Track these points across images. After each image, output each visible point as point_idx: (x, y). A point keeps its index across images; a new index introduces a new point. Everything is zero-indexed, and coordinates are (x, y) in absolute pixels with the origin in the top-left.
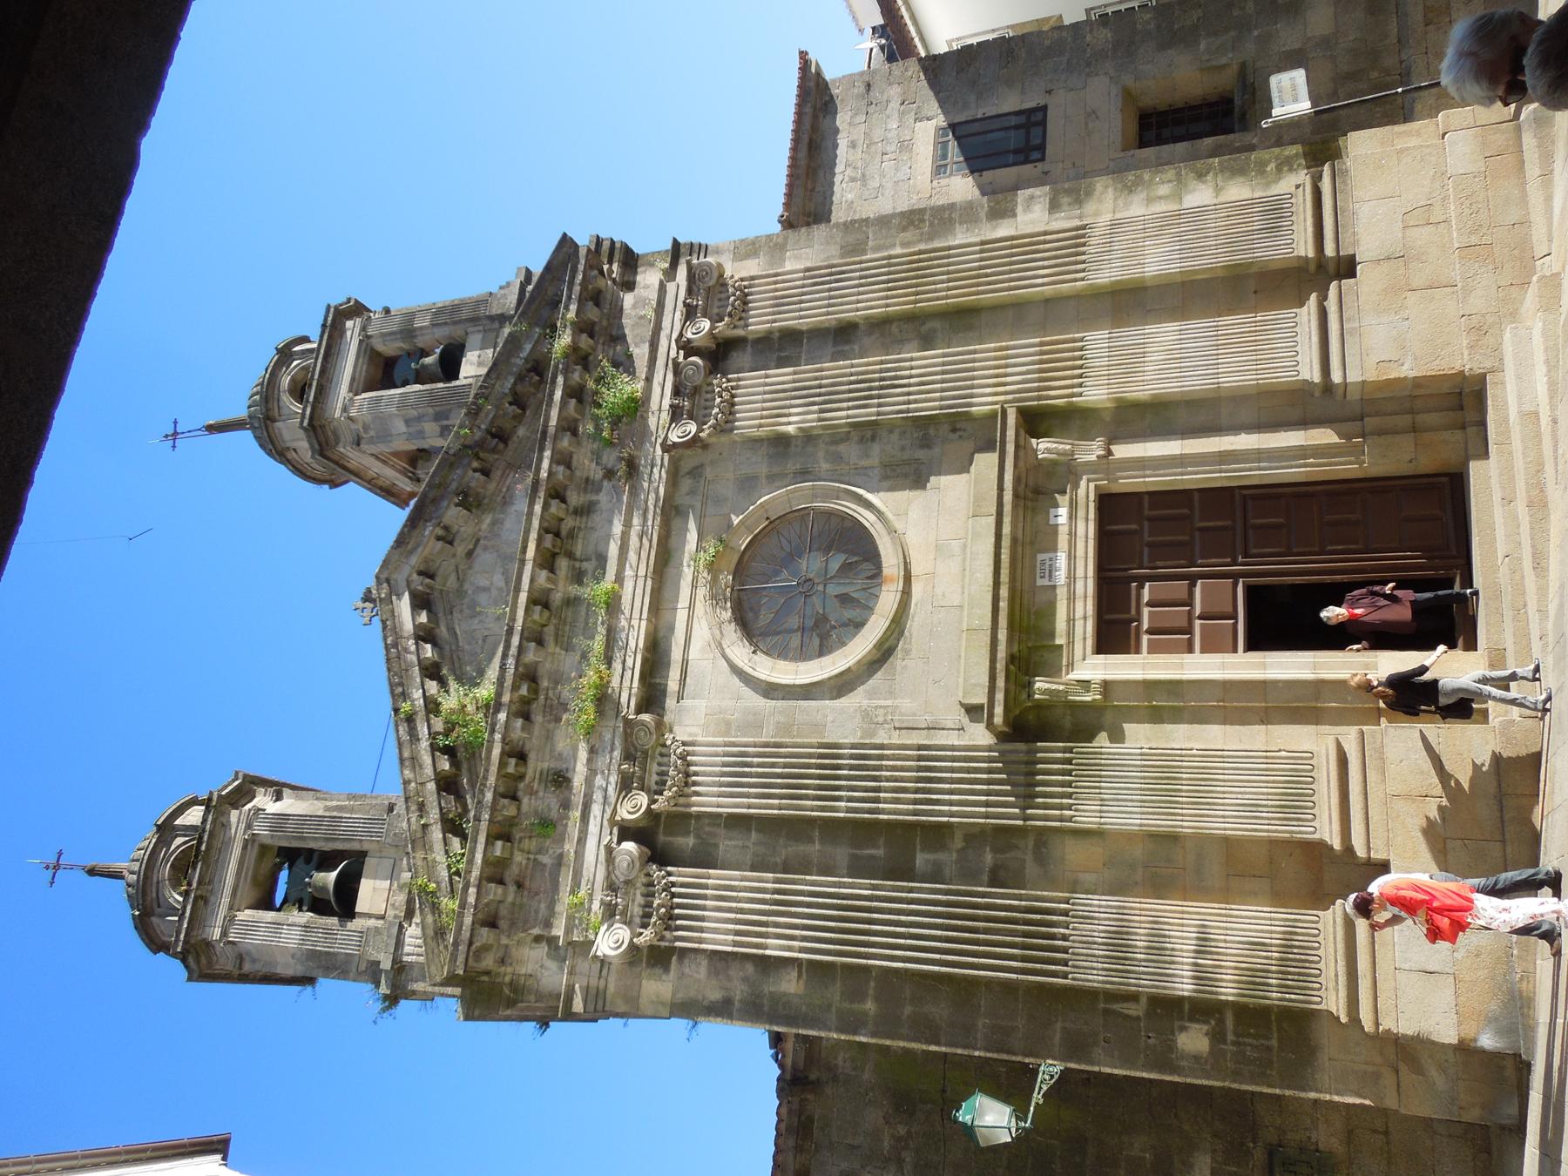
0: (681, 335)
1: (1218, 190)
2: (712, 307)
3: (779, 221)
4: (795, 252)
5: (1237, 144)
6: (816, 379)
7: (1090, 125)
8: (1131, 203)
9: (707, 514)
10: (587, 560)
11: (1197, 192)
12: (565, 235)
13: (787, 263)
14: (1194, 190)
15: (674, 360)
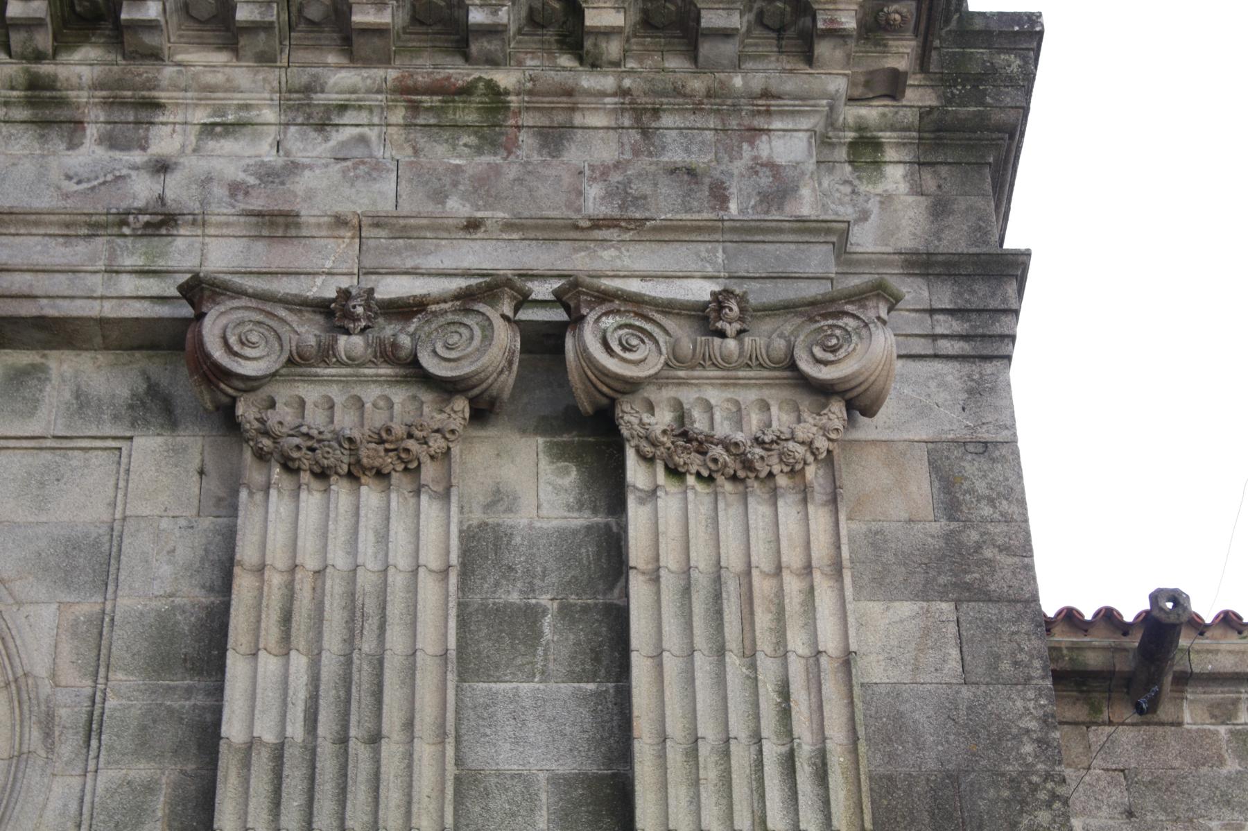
2: (726, 384)
4: (952, 629)
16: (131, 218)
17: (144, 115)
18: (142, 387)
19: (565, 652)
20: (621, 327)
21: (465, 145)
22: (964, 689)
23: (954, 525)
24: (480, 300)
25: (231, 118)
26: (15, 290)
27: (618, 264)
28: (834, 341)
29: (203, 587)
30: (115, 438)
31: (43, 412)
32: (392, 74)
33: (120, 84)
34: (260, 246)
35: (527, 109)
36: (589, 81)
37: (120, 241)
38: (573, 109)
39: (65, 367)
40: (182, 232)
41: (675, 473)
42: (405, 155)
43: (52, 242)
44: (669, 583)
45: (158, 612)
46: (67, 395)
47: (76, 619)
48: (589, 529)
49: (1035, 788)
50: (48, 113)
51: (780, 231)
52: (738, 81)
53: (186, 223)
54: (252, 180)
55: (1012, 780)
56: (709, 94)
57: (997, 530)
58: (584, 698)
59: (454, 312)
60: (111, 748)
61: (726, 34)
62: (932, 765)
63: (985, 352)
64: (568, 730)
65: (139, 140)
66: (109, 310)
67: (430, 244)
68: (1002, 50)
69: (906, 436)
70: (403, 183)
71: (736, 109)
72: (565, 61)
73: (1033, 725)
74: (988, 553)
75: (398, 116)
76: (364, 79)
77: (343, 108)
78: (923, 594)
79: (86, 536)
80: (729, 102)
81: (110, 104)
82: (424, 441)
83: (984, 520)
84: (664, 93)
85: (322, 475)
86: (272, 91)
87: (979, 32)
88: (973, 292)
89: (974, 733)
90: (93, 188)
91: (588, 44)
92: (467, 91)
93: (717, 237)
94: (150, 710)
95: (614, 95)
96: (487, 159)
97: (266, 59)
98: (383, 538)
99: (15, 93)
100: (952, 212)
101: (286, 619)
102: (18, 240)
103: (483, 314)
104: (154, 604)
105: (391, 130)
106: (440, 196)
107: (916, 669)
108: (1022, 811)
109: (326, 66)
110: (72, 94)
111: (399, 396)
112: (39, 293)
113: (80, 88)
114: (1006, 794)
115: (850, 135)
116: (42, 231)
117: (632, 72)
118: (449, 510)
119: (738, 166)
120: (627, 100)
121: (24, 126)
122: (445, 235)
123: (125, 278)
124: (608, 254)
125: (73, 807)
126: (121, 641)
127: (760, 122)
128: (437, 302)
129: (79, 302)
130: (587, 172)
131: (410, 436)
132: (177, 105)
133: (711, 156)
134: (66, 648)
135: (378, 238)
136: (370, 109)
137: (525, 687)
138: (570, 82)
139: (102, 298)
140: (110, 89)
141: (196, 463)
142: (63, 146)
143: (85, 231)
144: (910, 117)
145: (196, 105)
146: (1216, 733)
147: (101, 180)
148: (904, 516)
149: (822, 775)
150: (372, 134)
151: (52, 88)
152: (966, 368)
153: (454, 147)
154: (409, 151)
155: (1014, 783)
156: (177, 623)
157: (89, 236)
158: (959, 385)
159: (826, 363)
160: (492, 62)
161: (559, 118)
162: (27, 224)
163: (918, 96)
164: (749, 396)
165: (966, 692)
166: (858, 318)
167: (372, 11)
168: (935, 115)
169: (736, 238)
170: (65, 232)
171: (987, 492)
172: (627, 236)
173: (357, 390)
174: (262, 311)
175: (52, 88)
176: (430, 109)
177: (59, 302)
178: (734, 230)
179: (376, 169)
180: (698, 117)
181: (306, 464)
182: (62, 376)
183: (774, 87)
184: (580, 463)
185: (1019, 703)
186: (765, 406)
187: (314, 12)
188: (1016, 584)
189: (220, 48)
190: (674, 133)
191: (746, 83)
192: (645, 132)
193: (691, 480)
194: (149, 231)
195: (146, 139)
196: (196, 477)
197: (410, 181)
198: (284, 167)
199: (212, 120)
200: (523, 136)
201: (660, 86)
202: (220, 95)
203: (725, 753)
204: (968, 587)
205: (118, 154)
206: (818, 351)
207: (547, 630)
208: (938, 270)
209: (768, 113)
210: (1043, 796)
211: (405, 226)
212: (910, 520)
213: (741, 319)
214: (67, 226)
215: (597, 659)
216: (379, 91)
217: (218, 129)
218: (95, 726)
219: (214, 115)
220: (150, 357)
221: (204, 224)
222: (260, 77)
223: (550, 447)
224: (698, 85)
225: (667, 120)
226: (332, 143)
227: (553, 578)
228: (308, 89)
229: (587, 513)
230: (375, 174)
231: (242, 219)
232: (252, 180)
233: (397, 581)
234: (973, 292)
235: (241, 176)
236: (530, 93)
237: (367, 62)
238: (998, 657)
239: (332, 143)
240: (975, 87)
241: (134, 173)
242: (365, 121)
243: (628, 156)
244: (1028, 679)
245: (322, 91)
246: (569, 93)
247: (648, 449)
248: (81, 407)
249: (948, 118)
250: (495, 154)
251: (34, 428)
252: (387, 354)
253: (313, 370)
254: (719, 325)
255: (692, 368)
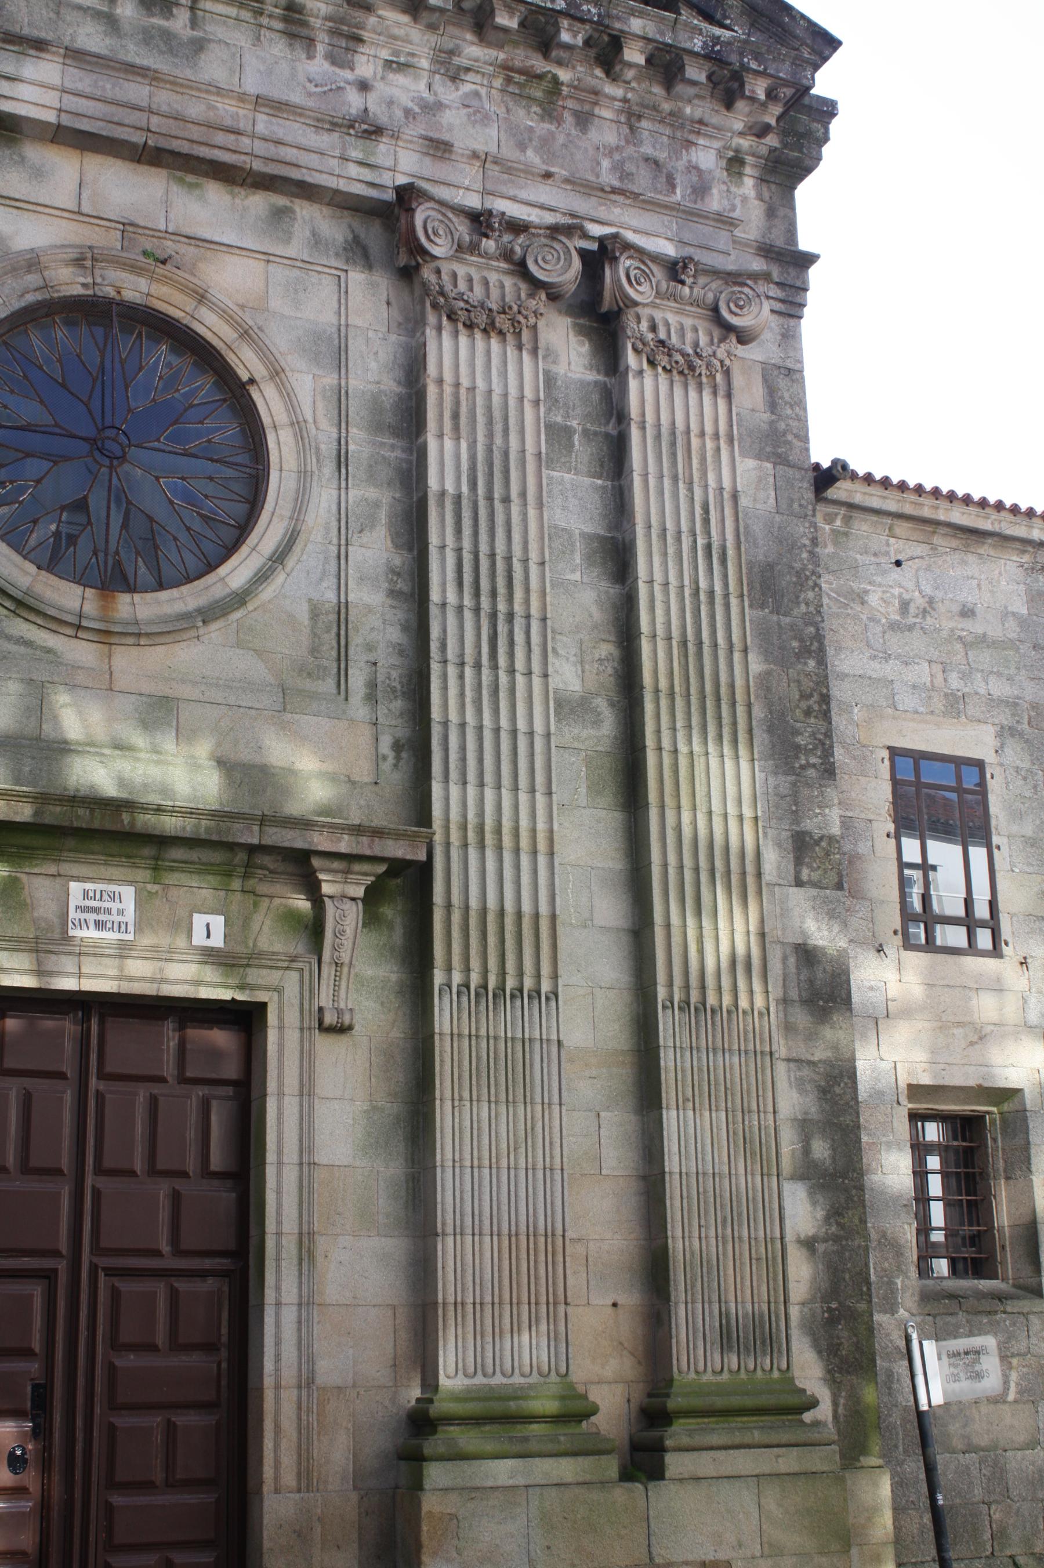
0: (627, 246)
1: (809, 1244)
2: (679, 312)
3: (835, 462)
4: (771, 480)
5: (899, 1282)
6: (523, 494)
7: (958, 1032)
8: (802, 1091)
9: (272, 267)
10: (194, 23)
11: (809, 1207)
12: (832, 44)
13: (751, 463)
14: (814, 1204)
15: (581, 228)
16: (357, 125)
17: (352, 44)
18: (350, 237)
19: (586, 459)
20: (638, 268)
21: (535, 113)
22: (777, 516)
23: (774, 417)
24: (562, 233)
25: (402, 60)
26: (288, 159)
27: (623, 219)
28: (742, 303)
29: (395, 380)
30: (336, 269)
31: (295, 242)
32: (502, 56)
33: (342, 21)
34: (427, 160)
35: (571, 97)
36: (611, 90)
37: (347, 137)
38: (596, 104)
39: (304, 212)
40: (384, 140)
41: (652, 363)
42: (502, 111)
43: (309, 130)
44: (650, 432)
45: (372, 392)
46: (308, 233)
47: (324, 387)
48: (596, 382)
49: (807, 578)
50: (295, 29)
51: (707, 218)
52: (688, 110)
53: (388, 135)
54: (417, 109)
55: (797, 572)
56: (671, 114)
57: (794, 424)
58: (596, 488)
59: (545, 237)
60: (354, 476)
61: (694, 83)
62: (761, 557)
63: (791, 312)
64: (589, 506)
65: (349, 62)
66: (343, 185)
67: (522, 181)
68: (815, 120)
69: (751, 357)
70: (502, 132)
71: (682, 126)
72: (599, 72)
73: (807, 542)
74: (790, 437)
75: (498, 83)
76: (485, 55)
77: (468, 70)
78: (758, 457)
79: (325, 331)
80: (680, 121)
81: (333, 32)
82: (526, 318)
83: (788, 417)
84: (646, 107)
85: (470, 326)
86: (430, 49)
87: (806, 106)
88: (788, 273)
89: (781, 542)
90: (325, 92)
91: (618, 68)
92: (540, 77)
93: (674, 213)
94: (372, 456)
95: (620, 101)
96: (546, 126)
97: (432, 27)
98: (504, 374)
99: (278, 11)
100: (776, 217)
101: (456, 416)
102: (288, 123)
103: (564, 244)
104: (369, 387)
105: (493, 91)
106: (522, 147)
107: (755, 500)
108: (801, 590)
109: (465, 40)
110: (312, 20)
111: (508, 282)
112: (302, 164)
113: (317, 17)
114: (794, 579)
115: (731, 154)
116: (302, 120)
117: (633, 89)
118: (537, 363)
119: (681, 164)
120: (627, 105)
121: (278, 34)
122: (531, 177)
123: (351, 165)
124: (617, 211)
125: (334, 508)
126: (355, 408)
127: (692, 137)
128: (536, 228)
129: (325, 176)
130: (602, 149)
131: (519, 312)
132: (373, 43)
133: (666, 154)
134: (320, 405)
135: (493, 170)
136: (483, 74)
137: (567, 476)
138: (599, 87)
139: (339, 176)
140: (335, 22)
141: (384, 297)
142: (304, 56)
143: (327, 126)
144: (764, 151)
145: (384, 46)
146: (824, 529)
147: (329, 87)
148: (750, 407)
149: (723, 560)
150: (483, 91)
151: (300, 13)
152: (782, 320)
153: (529, 113)
154: (504, 109)
155: (798, 574)
156: (383, 401)
157: (330, 130)
158: (777, 330)
159: (736, 314)
160: (560, 63)
161: (587, 107)
162: (295, 113)
163: (772, 140)
164: (688, 322)
165: (778, 518)
166: (754, 290)
167: (507, 17)
168: (777, 153)
169: (684, 217)
170: (316, 124)
171: (789, 400)
172: (628, 202)
173: (485, 273)
174: (440, 212)
175: (300, 13)
176: (517, 83)
177: (314, 173)
178: (684, 212)
179: (485, 119)
180: (661, 126)
181: (462, 319)
182: (303, 217)
183: (707, 118)
184: (590, 340)
185: (802, 529)
186: (695, 330)
187: (467, 5)
188: (801, 458)
189: (405, 12)
190: (647, 133)
191: (692, 112)
192: (631, 128)
193: (660, 369)
194: (365, 135)
195: (353, 61)
196: (385, 306)
197: (506, 131)
198: (435, 103)
199: (390, 58)
200: (567, 114)
201: (646, 102)
202: (399, 43)
203: (678, 539)
204: (779, 456)
205: (338, 70)
206: (732, 305)
207: (577, 443)
208: (773, 255)
209: (699, 133)
210: (811, 583)
211: (510, 167)
212: (753, 410)
213: (694, 276)
214: (318, 120)
215: (602, 466)
216: (491, 65)
217: (394, 66)
218: (342, 460)
219: (392, 55)
220: (353, 216)
221: (398, 138)
222: (426, 38)
223: (575, 325)
224: (666, 107)
225: (644, 124)
226: (460, 93)
227: (578, 411)
228: (451, 53)
229: (595, 373)
230: (486, 122)
231: (421, 141)
232: (417, 109)
233: (512, 402)
234: (788, 273)
235: (410, 105)
236: (575, 88)
237: (490, 45)
238: (792, 500)
239: (460, 93)
240: (798, 140)
241: (348, 87)
242: (479, 82)
243: (623, 143)
244: (806, 516)
245: (459, 56)
246: (596, 93)
247: (640, 346)
248: (316, 243)
249: (783, 156)
250: (551, 123)
251: (291, 252)
252: (507, 255)
253: (465, 256)
254: (683, 277)
255: (663, 299)
